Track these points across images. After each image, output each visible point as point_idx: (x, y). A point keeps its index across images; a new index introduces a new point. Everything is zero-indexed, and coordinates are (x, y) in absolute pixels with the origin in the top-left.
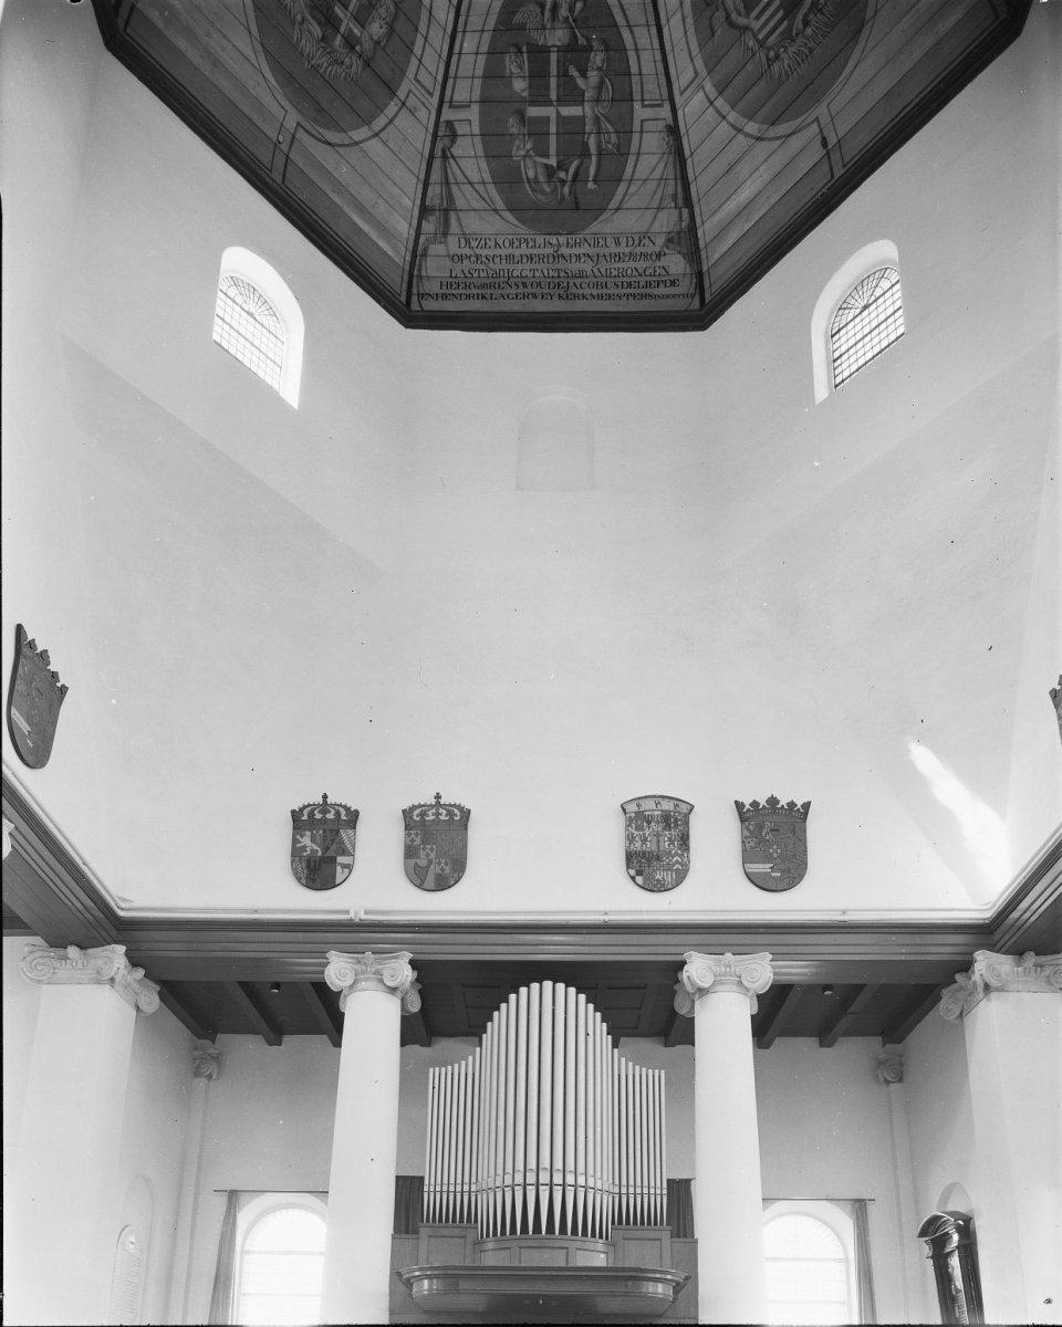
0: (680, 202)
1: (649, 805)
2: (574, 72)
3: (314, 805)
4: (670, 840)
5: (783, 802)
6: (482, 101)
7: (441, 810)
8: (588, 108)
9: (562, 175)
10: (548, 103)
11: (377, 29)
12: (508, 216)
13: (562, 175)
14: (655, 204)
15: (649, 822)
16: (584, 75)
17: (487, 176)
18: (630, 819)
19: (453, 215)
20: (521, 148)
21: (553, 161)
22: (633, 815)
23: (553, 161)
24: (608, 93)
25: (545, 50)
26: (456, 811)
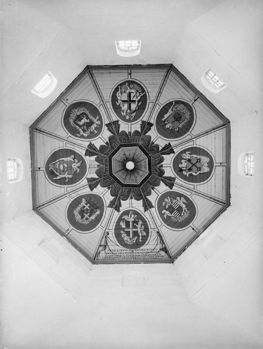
0: (162, 243)
11: (93, 217)
13: (133, 239)
23: (131, 237)
25: (129, 222)
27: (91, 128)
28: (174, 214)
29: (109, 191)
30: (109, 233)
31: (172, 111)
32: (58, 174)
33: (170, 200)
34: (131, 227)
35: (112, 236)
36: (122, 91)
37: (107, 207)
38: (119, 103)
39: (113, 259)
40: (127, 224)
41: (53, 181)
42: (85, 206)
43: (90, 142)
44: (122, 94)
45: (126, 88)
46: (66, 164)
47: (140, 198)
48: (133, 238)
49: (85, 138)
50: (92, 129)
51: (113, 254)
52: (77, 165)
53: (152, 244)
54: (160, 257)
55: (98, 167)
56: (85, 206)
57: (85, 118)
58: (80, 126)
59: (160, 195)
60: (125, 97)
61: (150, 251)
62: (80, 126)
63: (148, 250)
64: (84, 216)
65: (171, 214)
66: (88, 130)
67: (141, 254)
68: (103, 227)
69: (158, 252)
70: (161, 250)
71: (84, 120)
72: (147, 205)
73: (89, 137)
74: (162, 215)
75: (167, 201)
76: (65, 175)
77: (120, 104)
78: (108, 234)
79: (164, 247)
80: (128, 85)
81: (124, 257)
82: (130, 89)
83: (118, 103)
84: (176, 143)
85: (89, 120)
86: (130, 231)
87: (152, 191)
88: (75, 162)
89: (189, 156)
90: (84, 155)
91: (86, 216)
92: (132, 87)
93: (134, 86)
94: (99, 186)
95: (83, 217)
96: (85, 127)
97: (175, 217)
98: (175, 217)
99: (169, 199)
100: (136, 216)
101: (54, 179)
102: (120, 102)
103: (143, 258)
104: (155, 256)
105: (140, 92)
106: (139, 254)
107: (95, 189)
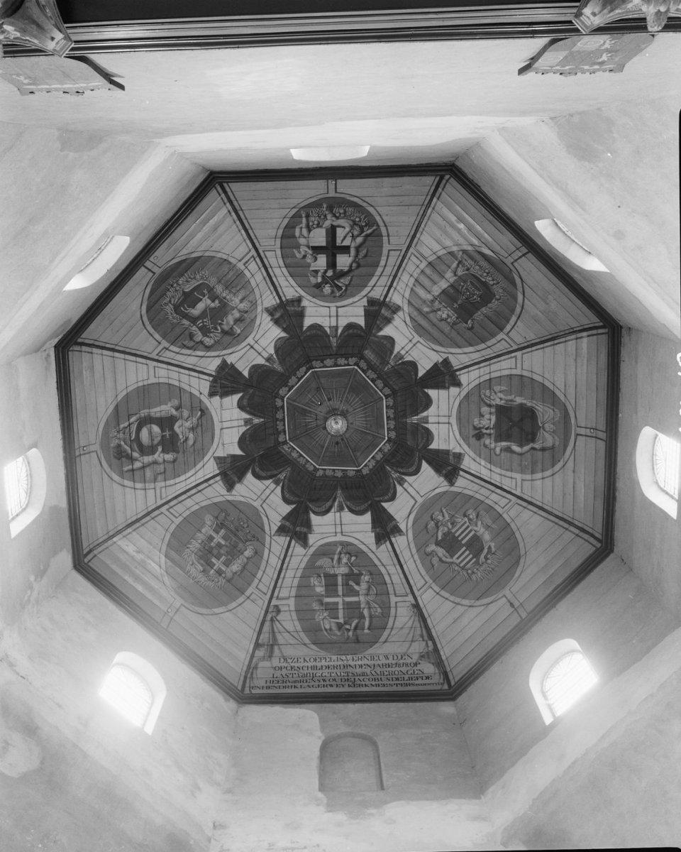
0: (426, 638)
2: (351, 583)
8: (362, 598)
9: (348, 627)
10: (338, 596)
11: (235, 567)
14: (410, 638)
16: (358, 584)
17: (299, 628)
21: (341, 621)
27: (224, 323)
28: (458, 558)
29: (279, 489)
30: (282, 608)
31: (455, 275)
32: (136, 455)
33: (447, 517)
34: (340, 593)
35: (289, 621)
36: (311, 224)
37: (274, 535)
38: (303, 253)
39: (295, 687)
41: (122, 475)
42: (214, 535)
43: (221, 358)
44: (309, 231)
45: (322, 217)
46: (157, 425)
47: (363, 507)
49: (208, 348)
50: (228, 323)
51: (293, 672)
52: (188, 424)
54: (420, 681)
55: (245, 425)
56: (214, 535)
57: (207, 297)
58: (194, 320)
59: (420, 500)
60: (319, 237)
61: (394, 662)
62: (194, 320)
63: (387, 658)
64: (211, 565)
65: (452, 557)
66: (216, 329)
67: (368, 670)
68: (264, 593)
69: (416, 664)
70: (422, 657)
72: (385, 528)
74: (426, 556)
75: (440, 518)
76: (156, 456)
77: (305, 257)
79: (430, 649)
80: (327, 208)
81: (324, 680)
82: (334, 219)
83: (300, 252)
84: (465, 360)
85: (217, 302)
87: (399, 488)
88: (181, 417)
89: (501, 399)
90: (207, 394)
91: (218, 564)
92: (340, 214)
93: (345, 210)
94: (249, 476)
96: (207, 321)
97: (461, 565)
98: (461, 565)
99: (446, 515)
101: (126, 469)
102: (307, 250)
103: (374, 683)
105: (364, 224)
106: (363, 670)
107: (238, 487)
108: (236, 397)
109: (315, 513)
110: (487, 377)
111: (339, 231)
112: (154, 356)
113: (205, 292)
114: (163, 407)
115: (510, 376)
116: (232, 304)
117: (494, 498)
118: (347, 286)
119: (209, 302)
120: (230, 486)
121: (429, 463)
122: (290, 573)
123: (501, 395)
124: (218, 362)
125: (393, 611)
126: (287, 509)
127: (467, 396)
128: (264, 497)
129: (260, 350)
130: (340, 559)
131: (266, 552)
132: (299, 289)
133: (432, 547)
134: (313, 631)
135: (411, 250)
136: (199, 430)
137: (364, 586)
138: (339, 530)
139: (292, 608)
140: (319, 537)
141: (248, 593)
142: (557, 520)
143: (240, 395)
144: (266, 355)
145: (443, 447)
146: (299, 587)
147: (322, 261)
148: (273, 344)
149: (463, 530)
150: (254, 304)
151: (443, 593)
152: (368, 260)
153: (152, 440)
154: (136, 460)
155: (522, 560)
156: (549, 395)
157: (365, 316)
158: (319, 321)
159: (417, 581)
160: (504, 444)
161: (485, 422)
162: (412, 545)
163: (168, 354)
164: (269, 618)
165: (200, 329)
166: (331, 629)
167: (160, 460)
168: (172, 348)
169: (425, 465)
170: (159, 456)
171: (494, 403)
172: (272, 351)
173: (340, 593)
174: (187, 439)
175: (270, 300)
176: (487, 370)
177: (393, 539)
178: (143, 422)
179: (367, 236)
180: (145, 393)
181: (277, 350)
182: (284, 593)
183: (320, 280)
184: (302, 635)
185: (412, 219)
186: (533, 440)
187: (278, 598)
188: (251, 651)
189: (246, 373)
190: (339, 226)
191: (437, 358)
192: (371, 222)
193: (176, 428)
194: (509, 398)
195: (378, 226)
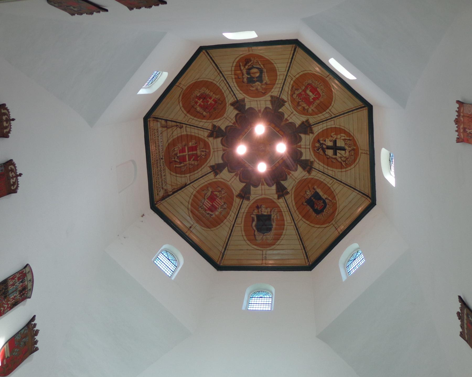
0: (173, 191)
1: (29, 277)
2: (194, 157)
3: (9, 115)
4: (15, 297)
5: (37, 338)
6: (187, 135)
7: (15, 178)
8: (188, 162)
9: (176, 158)
10: (188, 152)
11: (198, 109)
12: (167, 144)
13: (176, 158)
14: (173, 184)
15: (21, 282)
16: (194, 160)
17: (174, 137)
18: (22, 273)
19: (166, 129)
20: (180, 146)
21: (178, 155)
22: (24, 272)
23: (178, 155)
24: (191, 167)
25: (196, 150)
26: (15, 186)
32: (247, 67)
33: (223, 195)
34: (190, 153)
35: (177, 132)
40: (193, 149)
41: (238, 62)
42: (212, 99)
44: (344, 140)
48: (178, 157)
49: (292, 96)
50: (302, 104)
52: (259, 87)
53: (171, 179)
54: (156, 191)
56: (212, 99)
58: (305, 91)
60: (340, 143)
62: (305, 91)
63: (164, 176)
64: (199, 99)
65: (207, 199)
67: (159, 169)
69: (163, 188)
71: (312, 95)
73: (293, 100)
74: (207, 187)
75: (223, 192)
78: (181, 128)
83: (334, 135)
84: (289, 201)
85: (312, 100)
86: (185, 152)
87: (233, 174)
88: (262, 85)
91: (200, 102)
94: (236, 112)
95: (199, 98)
100: (204, 157)
101: (241, 63)
104: (157, 185)
107: (232, 108)
108: (270, 106)
109: (222, 139)
110: (282, 211)
111: (343, 152)
112: (289, 74)
113: (317, 96)
114: (267, 78)
115: (284, 220)
116: (311, 106)
117: (232, 215)
118: (319, 153)
119: (312, 97)
120: (232, 104)
121: (245, 186)
122: (196, 131)
123: (275, 217)
124: (286, 99)
125: (183, 176)
126: (223, 128)
127: (274, 202)
128: (228, 118)
129: (291, 116)
130: (203, 151)
131: (205, 121)
132: (317, 133)
133: (210, 190)
134: (173, 144)
135: (335, 180)
136: (257, 92)
137: (193, 162)
138: (215, 150)
139: (182, 134)
140: (212, 142)
141: (188, 115)
142: (226, 243)
143: (271, 108)
144: (288, 118)
145: (252, 192)
146: (191, 136)
147: (330, 144)
148: (293, 121)
149: (219, 202)
150: (311, 115)
151: (192, 196)
152: (329, 162)
153: (253, 73)
154: (244, 67)
155: (209, 229)
156: (278, 237)
157: (306, 160)
158: (303, 140)
159: (196, 184)
160: (255, 218)
161: (263, 209)
162: (211, 181)
163: (289, 80)
164: (178, 124)
165: (300, 94)
166: (175, 151)
167: (244, 77)
168: (292, 82)
169: (244, 184)
170: (246, 76)
171: (272, 213)
172: (290, 121)
173: (190, 153)
174: (253, 87)
175: (312, 121)
176: (286, 210)
177: (212, 173)
178: (261, 71)
179: (341, 163)
180: (273, 71)
181: (291, 123)
182: (188, 129)
183: (321, 142)
184: (172, 139)
185: (349, 182)
186: (258, 231)
187: (186, 127)
188: (164, 118)
189: (280, 110)
190: (345, 152)
191: (289, 189)
192: (348, 165)
193: (257, 83)
194: (275, 220)
195: (346, 168)
